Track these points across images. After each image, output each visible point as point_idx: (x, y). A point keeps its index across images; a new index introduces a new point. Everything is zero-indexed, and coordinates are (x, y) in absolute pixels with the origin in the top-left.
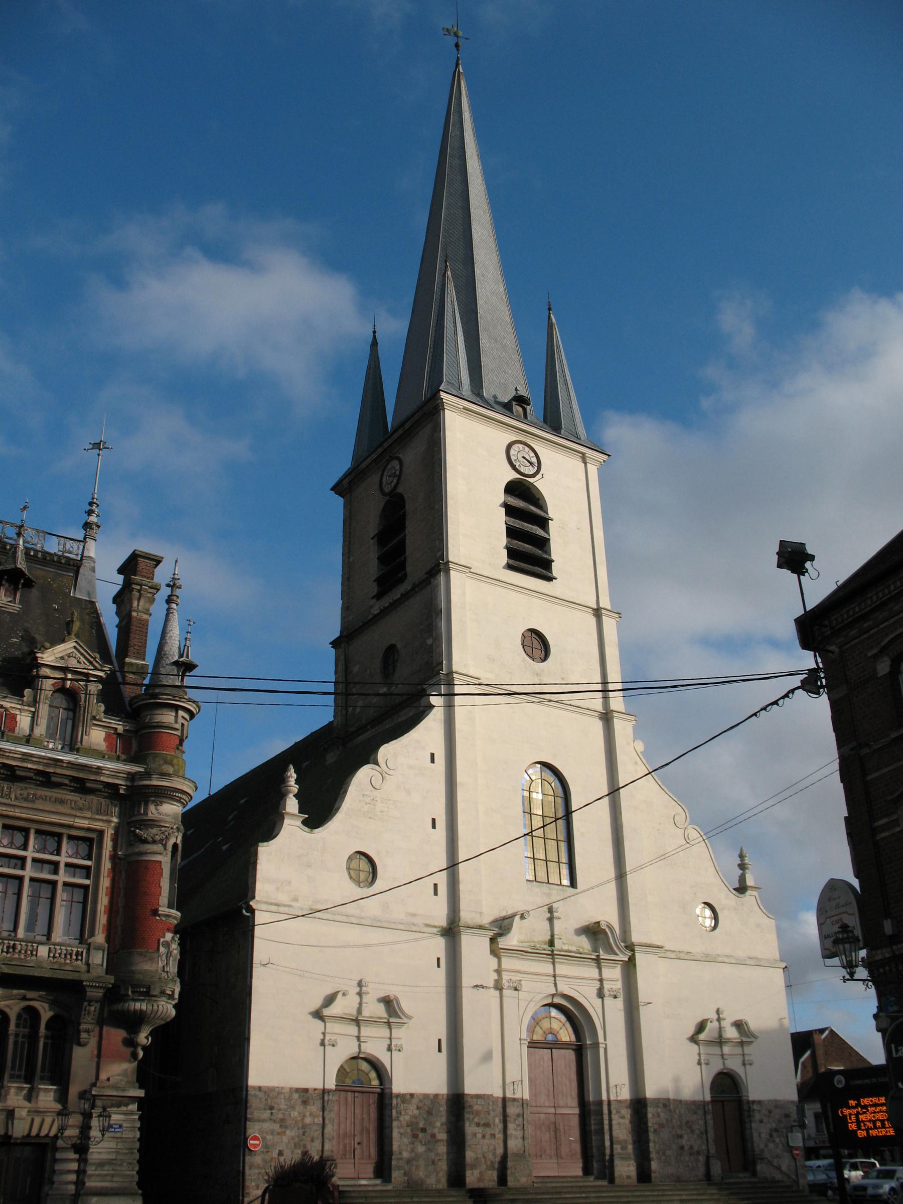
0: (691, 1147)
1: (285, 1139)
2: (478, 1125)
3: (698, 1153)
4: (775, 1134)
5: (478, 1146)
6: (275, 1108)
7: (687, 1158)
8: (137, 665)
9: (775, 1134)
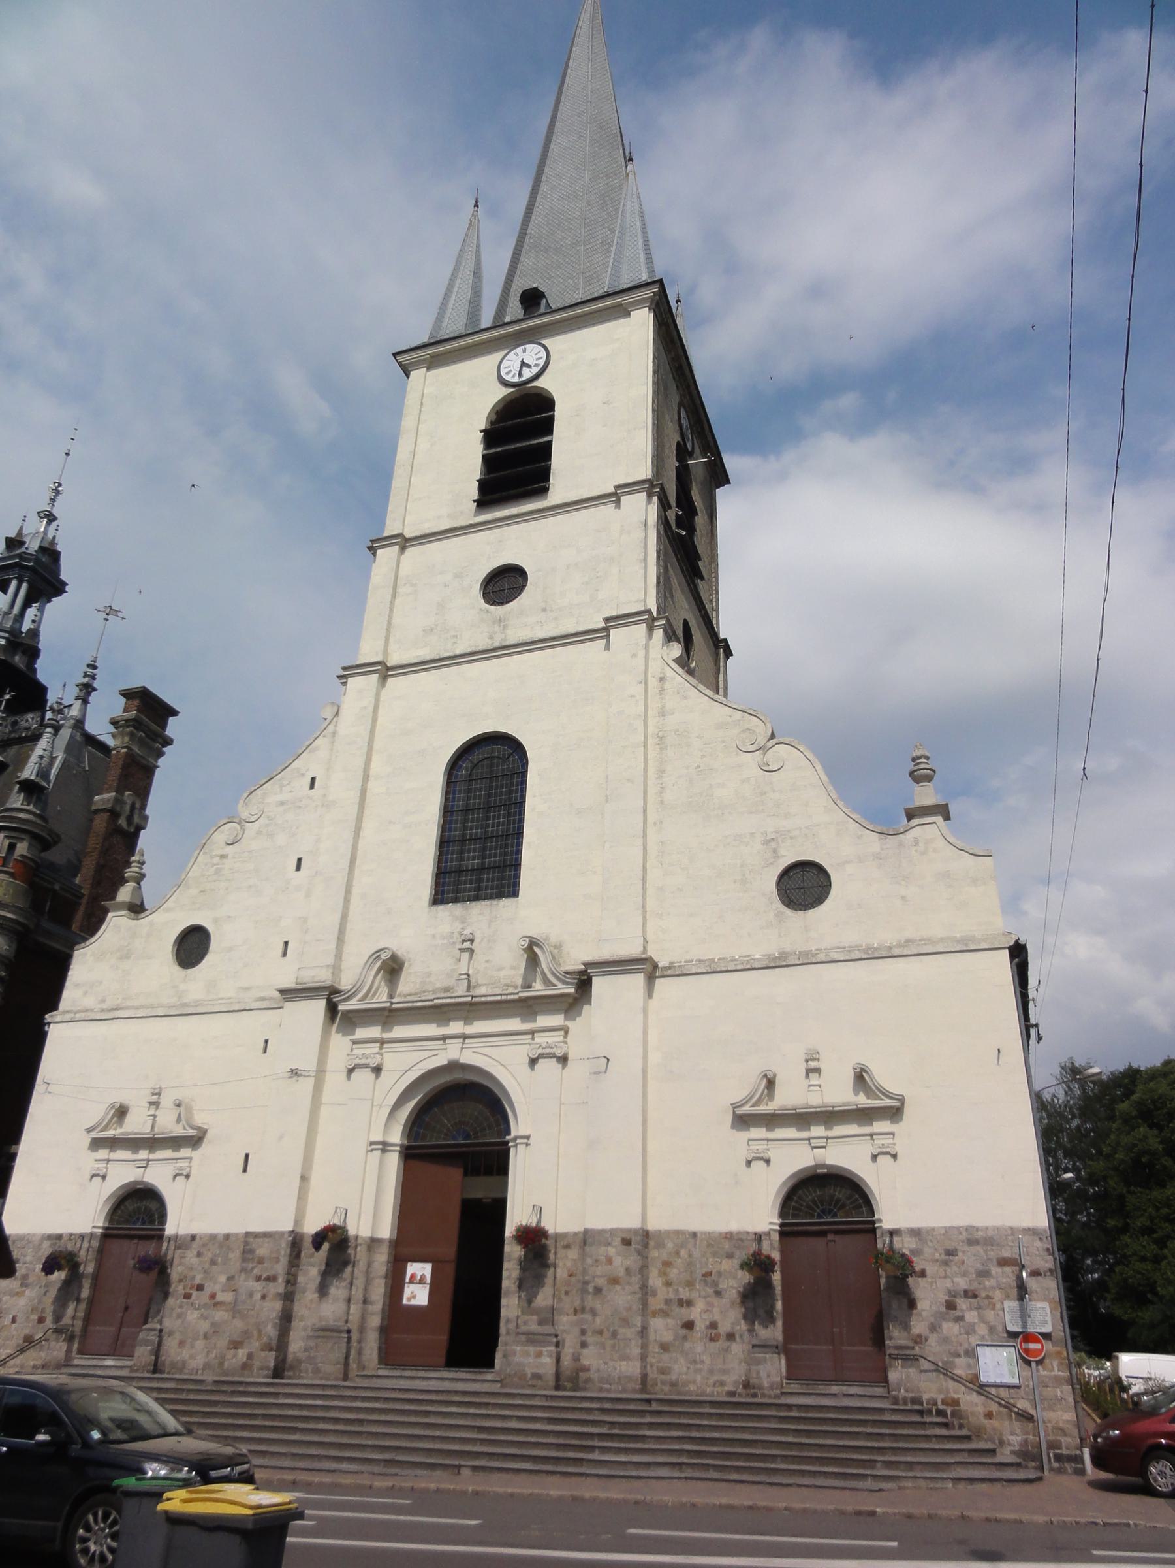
0: (713, 1325)
1: (22, 1302)
2: (258, 1279)
3: (731, 1337)
4: (962, 1304)
5: (252, 1312)
6: (21, 1261)
7: (699, 1348)
8: (146, 716)
9: (962, 1304)
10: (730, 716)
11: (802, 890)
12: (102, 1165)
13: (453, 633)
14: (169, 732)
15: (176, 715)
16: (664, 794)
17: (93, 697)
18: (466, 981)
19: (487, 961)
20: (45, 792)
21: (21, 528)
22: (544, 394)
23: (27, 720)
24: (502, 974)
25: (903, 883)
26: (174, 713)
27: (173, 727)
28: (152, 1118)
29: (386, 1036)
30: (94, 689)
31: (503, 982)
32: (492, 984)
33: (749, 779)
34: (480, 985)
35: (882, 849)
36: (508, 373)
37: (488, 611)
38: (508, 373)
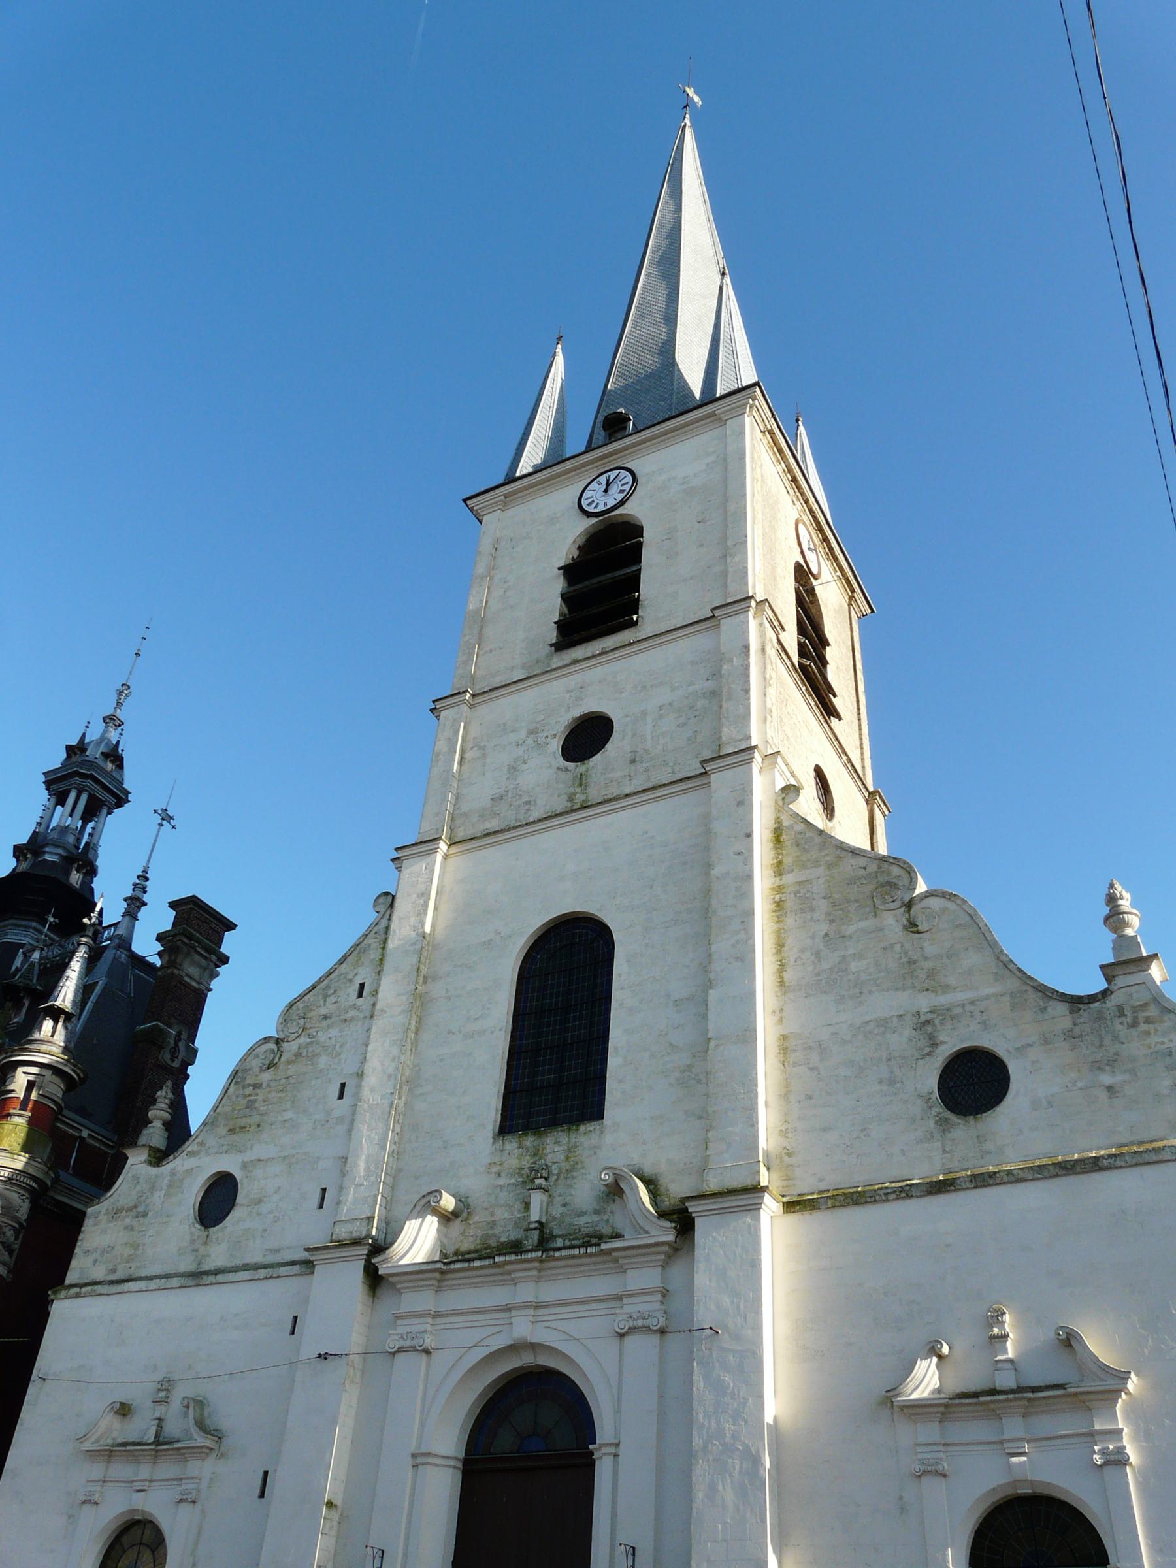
10: (865, 868)
11: (972, 1088)
12: (97, 1488)
13: (525, 799)
14: (224, 949)
15: (234, 929)
16: (784, 973)
17: (143, 913)
18: (537, 1232)
19: (564, 1205)
20: (9, 1004)
21: (84, 735)
22: (632, 522)
23: (73, 944)
24: (582, 1221)
25: (1107, 1068)
26: (231, 926)
27: (230, 944)
28: (157, 1422)
29: (444, 1307)
30: (144, 904)
31: (585, 1231)
32: (571, 1235)
33: (892, 946)
34: (556, 1237)
35: (1075, 1025)
36: (589, 505)
37: (567, 770)
38: (589, 505)
